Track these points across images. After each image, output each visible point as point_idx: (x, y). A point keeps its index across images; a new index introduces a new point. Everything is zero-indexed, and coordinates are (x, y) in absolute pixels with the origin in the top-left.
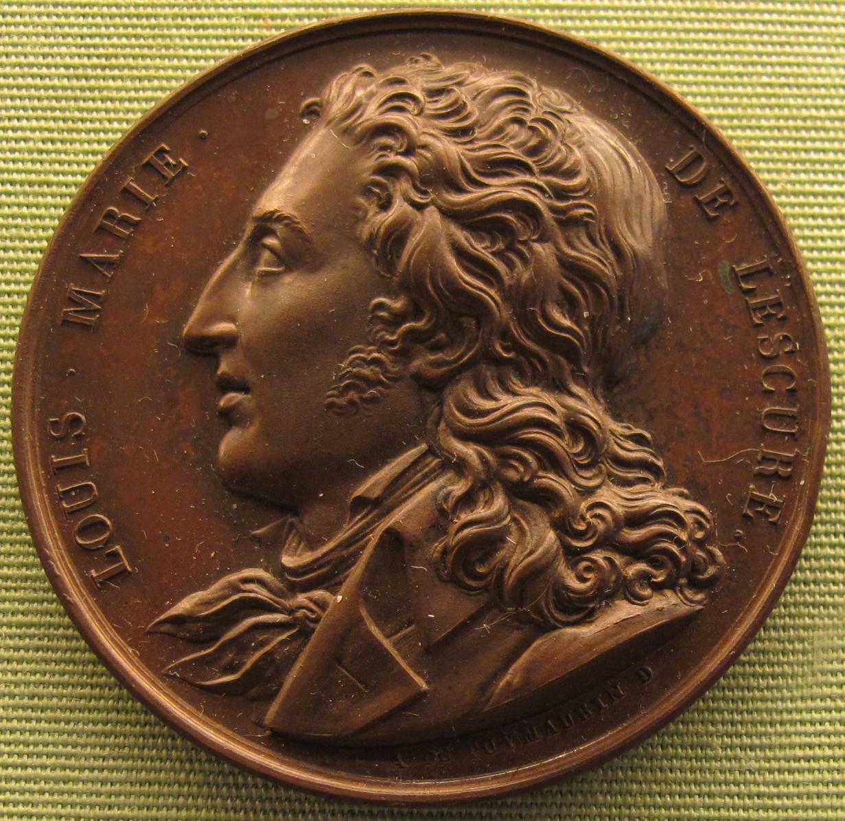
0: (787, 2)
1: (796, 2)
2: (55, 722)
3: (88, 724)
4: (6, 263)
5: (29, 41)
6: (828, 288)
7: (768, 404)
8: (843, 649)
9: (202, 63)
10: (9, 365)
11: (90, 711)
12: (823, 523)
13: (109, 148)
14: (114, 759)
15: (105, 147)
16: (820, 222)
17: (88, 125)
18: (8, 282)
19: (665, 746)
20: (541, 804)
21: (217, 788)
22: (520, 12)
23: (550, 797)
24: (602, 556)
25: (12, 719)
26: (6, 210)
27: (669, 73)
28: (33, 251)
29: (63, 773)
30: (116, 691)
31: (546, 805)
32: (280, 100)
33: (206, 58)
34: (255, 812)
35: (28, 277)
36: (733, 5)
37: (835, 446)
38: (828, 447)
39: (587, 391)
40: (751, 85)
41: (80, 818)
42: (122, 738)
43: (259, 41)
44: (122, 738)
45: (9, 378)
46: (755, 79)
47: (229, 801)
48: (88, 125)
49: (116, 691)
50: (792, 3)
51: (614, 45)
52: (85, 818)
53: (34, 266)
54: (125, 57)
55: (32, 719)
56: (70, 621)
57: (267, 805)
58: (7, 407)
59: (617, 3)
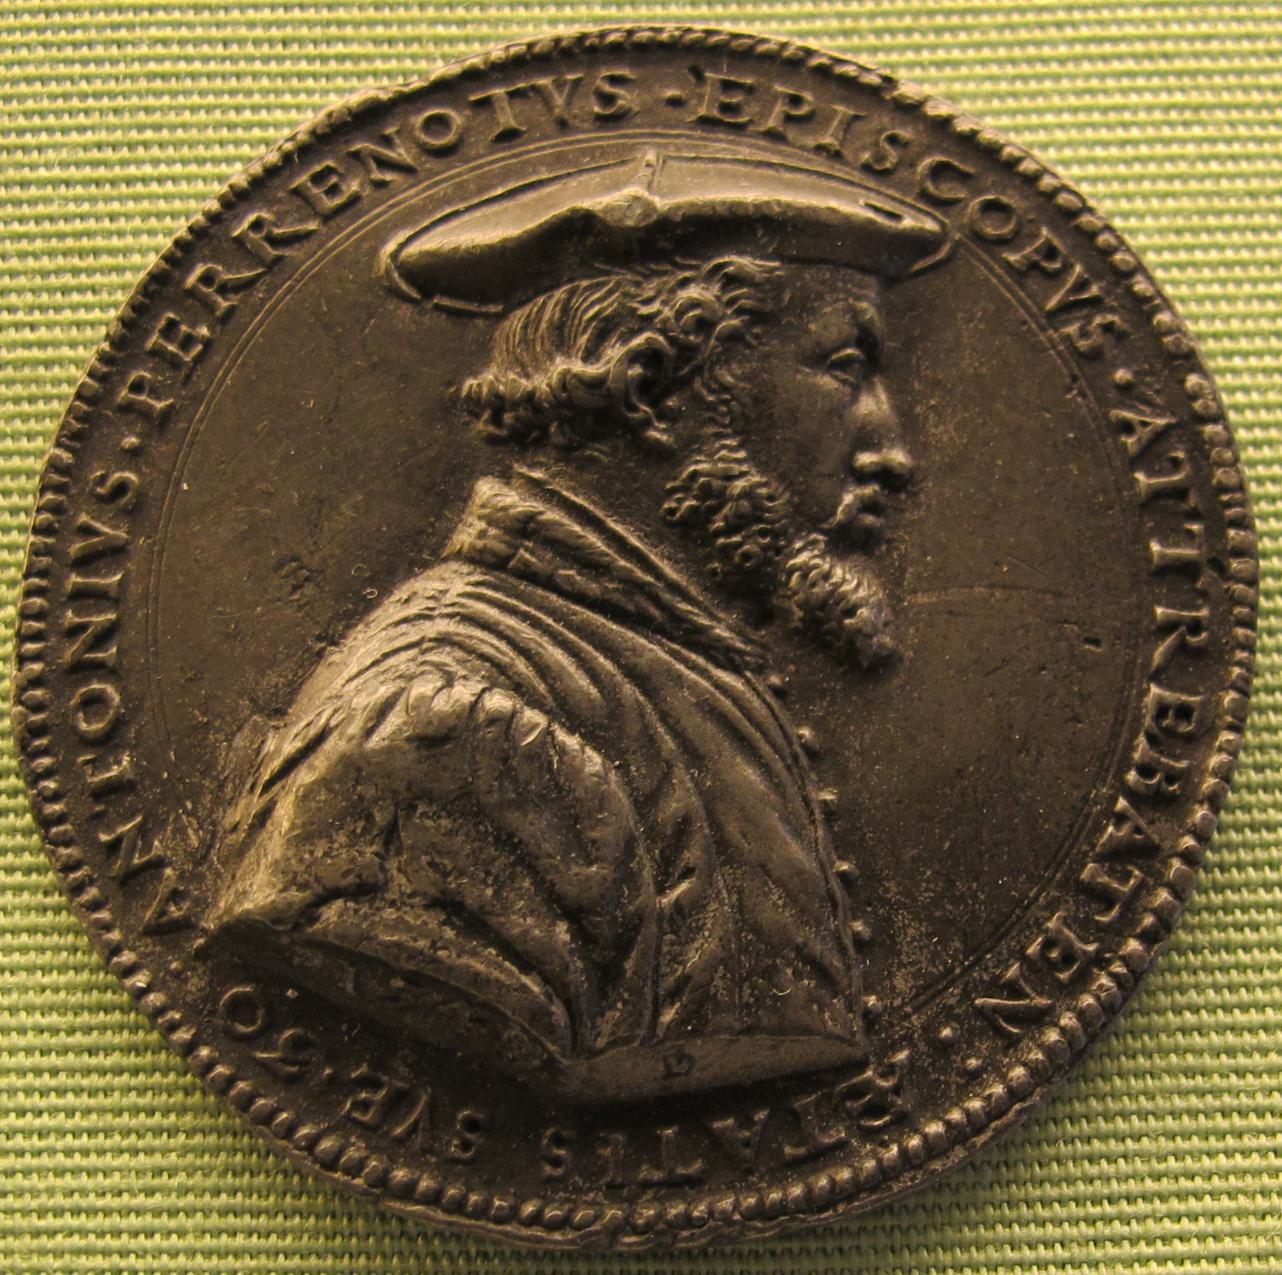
0: (656, 3)
1: (519, 4)
7: (125, 528)
16: (1260, 166)
18: (15, 436)
21: (350, 1219)
23: (923, 1215)
26: (9, 54)
29: (215, 1241)
30: (197, 1097)
31: (916, 1228)
34: (468, 1259)
36: (779, 9)
37: (1264, 699)
39: (416, 575)
41: (153, 1272)
42: (247, 1176)
43: (400, 80)
44: (247, 1176)
49: (197, 1097)
50: (664, 5)
52: (145, 1271)
55: (74, 1152)
57: (453, 1246)
59: (931, 5)
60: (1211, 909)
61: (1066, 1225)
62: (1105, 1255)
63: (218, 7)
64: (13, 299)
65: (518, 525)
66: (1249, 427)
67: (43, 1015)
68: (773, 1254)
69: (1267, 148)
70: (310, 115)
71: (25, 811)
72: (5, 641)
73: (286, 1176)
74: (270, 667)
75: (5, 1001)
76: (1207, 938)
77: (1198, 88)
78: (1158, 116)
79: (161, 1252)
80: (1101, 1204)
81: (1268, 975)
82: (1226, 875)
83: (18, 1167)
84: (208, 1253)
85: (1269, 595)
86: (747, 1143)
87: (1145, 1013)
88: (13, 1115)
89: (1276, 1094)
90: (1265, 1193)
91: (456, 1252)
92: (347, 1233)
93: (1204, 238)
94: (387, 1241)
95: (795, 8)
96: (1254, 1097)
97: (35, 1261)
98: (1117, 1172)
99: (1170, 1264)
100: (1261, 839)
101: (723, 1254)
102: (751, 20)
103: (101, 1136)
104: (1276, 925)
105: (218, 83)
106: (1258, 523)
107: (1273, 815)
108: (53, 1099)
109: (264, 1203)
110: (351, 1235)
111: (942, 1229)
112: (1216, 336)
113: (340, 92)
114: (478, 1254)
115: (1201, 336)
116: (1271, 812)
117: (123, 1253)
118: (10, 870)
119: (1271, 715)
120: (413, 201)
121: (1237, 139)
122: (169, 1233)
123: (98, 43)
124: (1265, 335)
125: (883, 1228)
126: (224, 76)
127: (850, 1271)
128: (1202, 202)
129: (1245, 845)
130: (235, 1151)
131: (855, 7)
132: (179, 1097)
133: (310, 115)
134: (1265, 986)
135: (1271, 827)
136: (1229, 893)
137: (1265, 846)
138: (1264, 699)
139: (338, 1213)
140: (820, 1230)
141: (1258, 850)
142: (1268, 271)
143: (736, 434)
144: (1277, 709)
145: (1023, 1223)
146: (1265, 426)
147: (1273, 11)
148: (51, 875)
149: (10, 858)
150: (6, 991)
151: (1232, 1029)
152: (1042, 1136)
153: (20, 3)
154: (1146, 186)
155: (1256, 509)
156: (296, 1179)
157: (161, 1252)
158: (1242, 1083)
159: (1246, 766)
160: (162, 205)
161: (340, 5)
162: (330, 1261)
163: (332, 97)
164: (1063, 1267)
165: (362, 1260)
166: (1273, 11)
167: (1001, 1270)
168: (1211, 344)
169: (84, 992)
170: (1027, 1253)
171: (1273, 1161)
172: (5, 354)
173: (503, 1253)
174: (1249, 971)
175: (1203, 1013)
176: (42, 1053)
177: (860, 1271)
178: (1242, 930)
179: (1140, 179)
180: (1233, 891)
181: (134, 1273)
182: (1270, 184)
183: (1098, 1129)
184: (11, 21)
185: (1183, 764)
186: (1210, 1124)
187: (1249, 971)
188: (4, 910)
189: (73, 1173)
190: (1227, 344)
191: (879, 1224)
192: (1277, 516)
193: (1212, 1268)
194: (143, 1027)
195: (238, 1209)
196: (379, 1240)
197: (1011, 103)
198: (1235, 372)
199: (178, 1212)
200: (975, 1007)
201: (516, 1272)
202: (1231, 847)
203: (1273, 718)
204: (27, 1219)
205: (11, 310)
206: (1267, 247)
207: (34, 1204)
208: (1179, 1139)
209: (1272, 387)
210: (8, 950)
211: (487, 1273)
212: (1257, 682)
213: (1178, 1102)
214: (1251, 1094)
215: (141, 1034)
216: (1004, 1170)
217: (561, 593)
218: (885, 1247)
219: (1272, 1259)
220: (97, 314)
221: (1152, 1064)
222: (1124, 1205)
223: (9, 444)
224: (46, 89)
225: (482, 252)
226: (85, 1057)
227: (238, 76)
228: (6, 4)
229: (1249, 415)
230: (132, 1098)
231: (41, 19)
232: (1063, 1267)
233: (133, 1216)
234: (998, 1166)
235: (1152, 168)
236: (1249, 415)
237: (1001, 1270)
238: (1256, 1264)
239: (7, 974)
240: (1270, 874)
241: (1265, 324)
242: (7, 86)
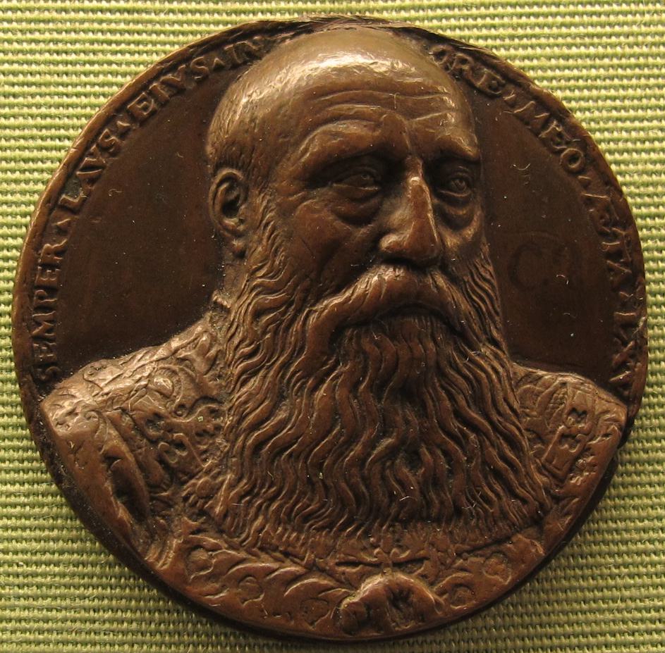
2: (40, 529)
3: (68, 566)
4: (6, 417)
9: (181, 38)
10: (8, 341)
12: (651, 386)
13: (106, 100)
15: (84, 121)
16: (529, 31)
17: (114, 47)
22: (403, 14)
25: (10, 471)
27: (523, 58)
32: (122, 120)
33: (173, 44)
35: (32, 208)
37: (655, 366)
38: (647, 287)
40: (577, 68)
45: (9, 308)
48: (114, 47)
51: (545, 83)
53: (12, 274)
54: (76, 74)
56: (56, 488)
65: (272, 47)
69: (656, 71)
71: (11, 370)
93: (608, 29)
100: (586, 618)
104: (662, 66)
107: (661, 455)
131: (32, 4)
135: (659, 462)
136: (644, 556)
138: (655, 366)
139: (172, 610)
143: (376, 183)
144: (662, 449)
147: (5, 647)
161: (570, 3)
179: (577, 79)
189: (28, 586)
196: (194, 625)
200: (505, 101)
204: (18, 164)
210: (5, 237)
228: (5, 4)
236: (639, 200)
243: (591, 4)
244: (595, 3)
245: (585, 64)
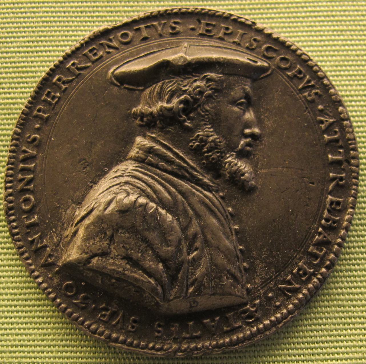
5: (9, 16)
6: (359, 124)
8: (364, 329)
11: (67, 335)
14: (91, 359)
19: (289, 332)
20: (259, 351)
21: (100, 348)
24: (177, 29)
28: (7, 130)
37: (361, 199)
40: (352, 353)
41: (44, 363)
42: (70, 336)
43: (114, 23)
44: (70, 336)
46: (327, 53)
47: (113, 360)
52: (41, 363)
58: (5, 221)
59: (266, 1)
60: (346, 259)
61: (304, 350)
62: (316, 358)
63: (62, 2)
64: (4, 85)
65: (148, 150)
66: (357, 122)
67: (12, 290)
68: (221, 358)
69: (362, 42)
70: (88, 33)
71: (7, 232)
72: (1, 183)
73: (82, 336)
74: (77, 190)
75: (1, 286)
76: (345, 268)
77: (342, 25)
78: (330, 33)
79: (46, 358)
80: (314, 344)
81: (362, 278)
82: (350, 250)
83: (5, 333)
84: (59, 358)
85: (362, 170)
86: (213, 326)
87: (327, 289)
88: (4, 318)
89: (364, 312)
90: (361, 341)
91: (130, 358)
92: (99, 352)
93: (344, 68)
94: (110, 354)
95: (227, 2)
96: (358, 313)
97: (10, 360)
98: (319, 335)
99: (334, 361)
100: (360, 239)
101: (206, 358)
102: (214, 6)
103: (29, 324)
105: (62, 24)
106: (359, 149)
107: (363, 233)
108: (15, 314)
109: (75, 344)
110: (100, 352)
111: (269, 351)
112: (347, 96)
113: (97, 26)
114: (136, 358)
115: (343, 96)
116: (363, 232)
117: (35, 358)
118: (3, 248)
119: (363, 204)
120: (118, 57)
121: (353, 40)
122: (48, 352)
123: (28, 12)
124: (361, 96)
125: (252, 351)
126: (64, 22)
127: (243, 363)
128: (343, 58)
129: (355, 241)
130: (67, 329)
132: (51, 313)
133: (88, 33)
134: (361, 282)
135: (363, 236)
136: (351, 255)
137: (361, 242)
138: (361, 199)
139: (97, 346)
140: (234, 351)
141: (359, 243)
142: (362, 77)
143: (210, 124)
144: (364, 202)
145: (292, 349)
146: (361, 122)
147: (363, 3)
148: (14, 250)
149: (3, 245)
150: (2, 283)
151: (352, 294)
152: (297, 324)
153: (6, 1)
154: (327, 53)
155: (358, 145)
156: (84, 337)
157: (46, 358)
158: (355, 309)
159: (356, 219)
160: (46, 59)
162: (94, 360)
163: (95, 28)
164: (304, 362)
165: (103, 360)
166: (363, 3)
167: (286, 363)
168: (346, 98)
169: (24, 283)
170: (293, 358)
171: (364, 331)
172: (1, 101)
173: (143, 358)
174: (357, 277)
175: (344, 289)
176: (12, 301)
177: (245, 363)
178: (354, 265)
180: (352, 254)
181: (38, 363)
182: (363, 53)
183: (313, 322)
184: (3, 6)
185: (338, 218)
186: (345, 321)
187: (357, 277)
188: (1, 260)
189: (21, 335)
190: (350, 98)
191: (251, 349)
192: (365, 147)
193: (346, 362)
194: (41, 293)
195: (68, 345)
196: (108, 354)
197: (289, 29)
198: (353, 106)
199: (51, 346)
200: (278, 288)
201: (147, 363)
202: (351, 242)
203: (363, 205)
205: (3, 88)
206: (362, 70)
207: (10, 344)
208: (336, 325)
209: (363, 111)
210: (2, 271)
211: (139, 363)
212: (359, 195)
213: (336, 315)
214: (357, 312)
215: (40, 295)
216: (287, 334)
217: (160, 169)
218: (253, 356)
219: (363, 359)
220: (28, 90)
221: (329, 304)
222: (321, 344)
223: (3, 127)
224: (13, 26)
225: (138, 72)
226: (24, 302)
227: (68, 22)
228: (2, 1)
229: (357, 119)
230: (38, 314)
231: (12, 5)
232: (304, 362)
233: (38, 347)
234: (285, 333)
235: (329, 48)
236: (357, 119)
237: (286, 363)
238: (359, 361)
239: (2, 278)
240: (362, 250)
241: (361, 93)
242: (2, 24)
243: (112, 2)
244: (114, 1)
245: (293, 6)
